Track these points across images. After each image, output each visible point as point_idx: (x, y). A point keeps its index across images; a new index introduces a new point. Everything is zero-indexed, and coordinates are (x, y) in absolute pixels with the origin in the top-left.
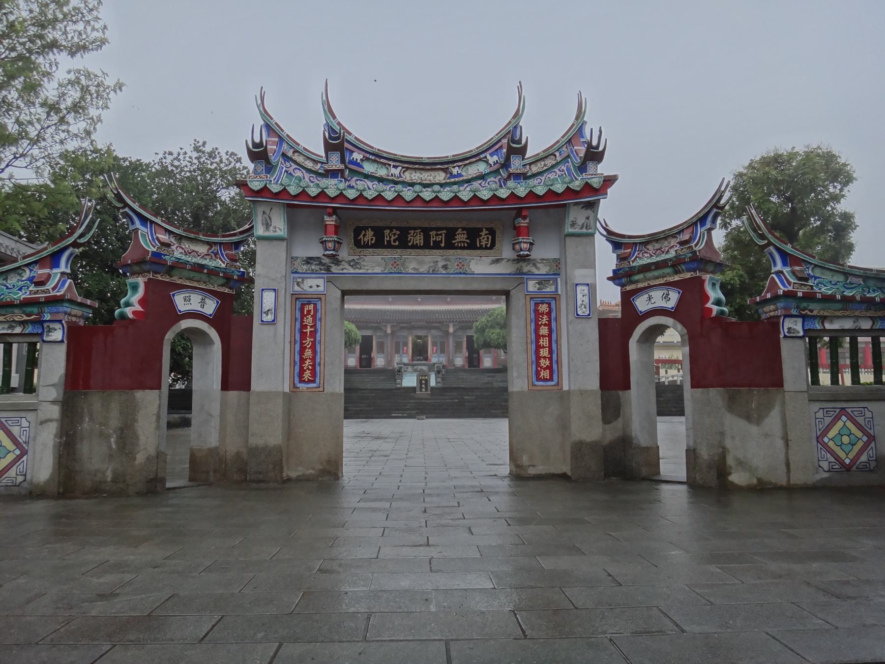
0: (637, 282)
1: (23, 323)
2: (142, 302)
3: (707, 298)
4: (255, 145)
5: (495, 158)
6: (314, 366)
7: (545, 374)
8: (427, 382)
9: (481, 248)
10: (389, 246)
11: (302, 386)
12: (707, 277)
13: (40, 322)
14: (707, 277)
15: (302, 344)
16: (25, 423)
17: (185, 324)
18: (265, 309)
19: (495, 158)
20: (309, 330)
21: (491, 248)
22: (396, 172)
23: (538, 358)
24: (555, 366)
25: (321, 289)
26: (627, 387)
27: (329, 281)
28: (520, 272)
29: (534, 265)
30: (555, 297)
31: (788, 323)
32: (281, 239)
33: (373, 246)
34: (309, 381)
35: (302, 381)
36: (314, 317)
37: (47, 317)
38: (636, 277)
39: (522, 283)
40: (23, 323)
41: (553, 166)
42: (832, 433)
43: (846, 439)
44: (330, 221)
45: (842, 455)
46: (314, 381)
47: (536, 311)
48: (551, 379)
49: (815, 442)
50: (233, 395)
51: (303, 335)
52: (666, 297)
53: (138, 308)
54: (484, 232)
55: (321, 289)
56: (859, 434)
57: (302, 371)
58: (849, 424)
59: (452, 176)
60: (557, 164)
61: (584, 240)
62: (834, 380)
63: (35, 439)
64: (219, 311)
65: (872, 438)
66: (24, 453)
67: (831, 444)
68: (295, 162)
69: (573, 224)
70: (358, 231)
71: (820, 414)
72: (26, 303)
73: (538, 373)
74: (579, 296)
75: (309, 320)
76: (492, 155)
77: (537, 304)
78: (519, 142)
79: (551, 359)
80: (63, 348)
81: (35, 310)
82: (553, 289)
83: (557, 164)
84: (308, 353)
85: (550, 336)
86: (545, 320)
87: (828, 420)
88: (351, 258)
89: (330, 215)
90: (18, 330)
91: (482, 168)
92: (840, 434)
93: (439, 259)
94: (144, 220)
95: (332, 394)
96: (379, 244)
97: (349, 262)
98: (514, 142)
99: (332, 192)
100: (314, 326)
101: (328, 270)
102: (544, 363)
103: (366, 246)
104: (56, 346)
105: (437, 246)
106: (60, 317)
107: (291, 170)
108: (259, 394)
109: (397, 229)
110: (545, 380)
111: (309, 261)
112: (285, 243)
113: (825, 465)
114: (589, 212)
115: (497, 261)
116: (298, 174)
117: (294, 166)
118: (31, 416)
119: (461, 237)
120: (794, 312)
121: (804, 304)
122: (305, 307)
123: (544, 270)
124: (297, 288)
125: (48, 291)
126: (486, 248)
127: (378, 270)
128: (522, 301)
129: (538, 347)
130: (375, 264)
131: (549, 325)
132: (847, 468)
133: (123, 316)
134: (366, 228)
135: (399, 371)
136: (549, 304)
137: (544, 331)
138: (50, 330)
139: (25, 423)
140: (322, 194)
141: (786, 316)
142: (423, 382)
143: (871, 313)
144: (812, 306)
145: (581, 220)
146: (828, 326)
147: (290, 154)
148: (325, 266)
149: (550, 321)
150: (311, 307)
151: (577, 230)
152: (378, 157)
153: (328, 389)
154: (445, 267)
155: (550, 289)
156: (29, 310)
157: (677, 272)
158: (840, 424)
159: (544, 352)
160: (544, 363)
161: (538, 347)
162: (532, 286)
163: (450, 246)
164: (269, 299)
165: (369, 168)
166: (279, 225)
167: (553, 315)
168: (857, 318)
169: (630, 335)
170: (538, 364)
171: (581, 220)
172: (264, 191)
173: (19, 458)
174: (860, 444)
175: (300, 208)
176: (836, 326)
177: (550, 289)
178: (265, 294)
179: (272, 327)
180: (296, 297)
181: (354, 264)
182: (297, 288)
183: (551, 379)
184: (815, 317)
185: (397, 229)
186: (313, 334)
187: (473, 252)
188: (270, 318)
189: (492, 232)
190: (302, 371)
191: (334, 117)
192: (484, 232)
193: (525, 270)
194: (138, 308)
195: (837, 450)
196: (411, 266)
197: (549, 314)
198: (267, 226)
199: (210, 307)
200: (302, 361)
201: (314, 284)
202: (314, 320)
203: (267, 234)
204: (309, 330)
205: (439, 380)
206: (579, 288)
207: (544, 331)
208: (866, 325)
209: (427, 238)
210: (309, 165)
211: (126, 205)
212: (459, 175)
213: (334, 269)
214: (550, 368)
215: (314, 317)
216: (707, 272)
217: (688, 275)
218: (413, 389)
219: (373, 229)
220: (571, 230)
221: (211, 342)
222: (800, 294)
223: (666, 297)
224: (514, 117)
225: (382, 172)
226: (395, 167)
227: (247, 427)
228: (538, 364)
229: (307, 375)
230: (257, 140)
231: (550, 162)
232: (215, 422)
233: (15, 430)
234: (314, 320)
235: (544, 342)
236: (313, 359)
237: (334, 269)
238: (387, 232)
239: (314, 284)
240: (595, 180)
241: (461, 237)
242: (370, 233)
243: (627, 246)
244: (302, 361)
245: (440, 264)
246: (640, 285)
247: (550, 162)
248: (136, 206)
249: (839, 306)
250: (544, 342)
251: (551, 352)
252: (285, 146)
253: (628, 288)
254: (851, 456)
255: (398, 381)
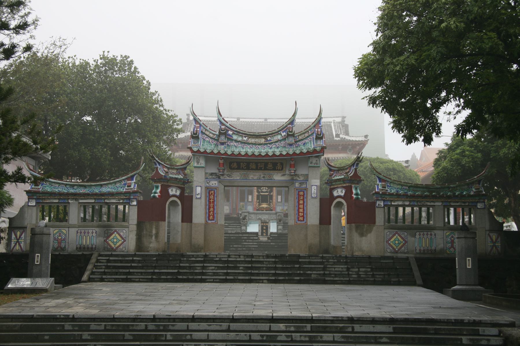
0: (334, 185)
1: (123, 199)
2: (160, 192)
3: (353, 193)
4: (194, 134)
5: (285, 133)
6: (214, 214)
7: (301, 219)
8: (267, 228)
9: (278, 170)
10: (243, 169)
11: (209, 222)
12: (353, 186)
13: (129, 199)
14: (353, 186)
15: (209, 206)
16: (125, 232)
17: (171, 199)
18: (197, 193)
19: (285, 133)
20: (212, 200)
21: (282, 169)
22: (245, 139)
23: (299, 212)
24: (305, 216)
25: (217, 185)
26: (330, 224)
27: (219, 182)
28: (292, 179)
29: (298, 177)
30: (306, 189)
31: (378, 203)
32: (203, 167)
33: (237, 169)
34: (212, 220)
35: (209, 220)
36: (214, 196)
37: (132, 197)
38: (334, 183)
39: (293, 184)
40: (123, 199)
41: (308, 137)
42: (392, 240)
43: (397, 242)
44: (221, 162)
45: (395, 247)
46: (214, 220)
47: (299, 194)
48: (303, 220)
49: (385, 243)
50: (185, 224)
51: (210, 203)
52: (176, 191)
53: (159, 194)
54: (279, 164)
55: (217, 185)
56: (402, 240)
57: (209, 216)
58: (399, 237)
59: (267, 140)
60: (309, 136)
61: (316, 169)
62: (428, 222)
63: (128, 237)
64: (181, 194)
65: (406, 242)
66: (125, 241)
67: (391, 243)
68: (206, 135)
69: (311, 163)
70: (231, 163)
71: (388, 233)
72: (126, 193)
73: (298, 218)
74: (313, 190)
75: (212, 197)
76: (283, 132)
77: (299, 192)
78: (292, 132)
79: (303, 213)
80: (136, 207)
81: (128, 195)
82: (305, 186)
83: (309, 136)
84: (212, 209)
85: (303, 204)
86: (302, 198)
87: (391, 236)
88: (228, 173)
89: (221, 160)
90: (121, 201)
91: (279, 137)
92: (395, 240)
93: (261, 174)
94: (159, 164)
95: (221, 225)
96: (239, 168)
97: (227, 175)
98: (290, 132)
99: (222, 152)
100: (214, 199)
101: (219, 178)
102: (301, 214)
103: (234, 169)
104: (134, 207)
105: (261, 169)
106: (136, 197)
107: (204, 138)
108: (195, 224)
109: (246, 162)
110: (301, 221)
111: (212, 174)
112: (204, 169)
113: (389, 250)
114: (317, 159)
115: (284, 175)
116: (207, 139)
117: (206, 136)
118: (127, 229)
119: (270, 166)
120: (380, 199)
121: (383, 196)
122: (210, 192)
123: (302, 178)
124: (207, 185)
125: (132, 189)
126: (280, 170)
127: (238, 178)
128: (293, 191)
129: (299, 208)
130: (237, 176)
131: (303, 200)
132: (397, 252)
133: (154, 197)
134: (234, 162)
135: (244, 219)
136: (304, 192)
137: (301, 202)
138: (132, 201)
139: (125, 232)
140: (219, 153)
141: (377, 200)
142: (264, 228)
143: (408, 199)
144: (386, 197)
145: (314, 162)
146: (393, 203)
147: (204, 131)
148: (217, 176)
149: (304, 198)
150: (213, 192)
151: (313, 165)
152: (238, 133)
153: (219, 223)
154: (264, 177)
155: (304, 186)
156: (126, 195)
157: (345, 183)
158: (395, 237)
159: (301, 210)
160: (301, 214)
161: (299, 208)
162: (297, 185)
163: (266, 169)
164: (199, 190)
165: (235, 137)
166: (202, 163)
167: (305, 196)
168: (404, 201)
169: (331, 205)
170: (299, 215)
171: (314, 162)
172: (198, 151)
173: (404, 244)
174: (402, 244)
175: (210, 157)
176: (396, 203)
177: (304, 186)
178: (197, 188)
179: (199, 200)
180: (207, 188)
181: (229, 176)
182: (207, 185)
183: (303, 220)
184: (388, 200)
185: (246, 162)
186: (213, 202)
187: (275, 171)
188: (199, 196)
189: (282, 164)
190: (209, 216)
191: (221, 116)
192: (279, 164)
193: (295, 178)
194: (159, 194)
195: (394, 246)
196: (251, 177)
197: (303, 196)
198: (198, 163)
199: (178, 193)
200: (209, 212)
201: (214, 183)
202: (214, 197)
203: (198, 166)
204: (212, 200)
205: (280, 227)
206: (313, 187)
207: (301, 202)
208: (407, 203)
209: (257, 166)
210: (211, 135)
211: (155, 159)
212: (270, 140)
213: (222, 178)
214: (303, 216)
215: (214, 196)
216: (354, 183)
217: (347, 185)
218: (256, 234)
219: (237, 162)
220: (311, 165)
221: (178, 205)
222: (381, 193)
223: (176, 191)
224: (293, 116)
225: (240, 139)
226: (245, 137)
227: (191, 236)
228: (299, 215)
229: (211, 218)
230: (195, 132)
231: (306, 135)
232: (180, 233)
233: (122, 234)
234: (214, 197)
235: (301, 206)
236: (214, 212)
237: (222, 178)
238: (242, 164)
239: (214, 183)
240: (318, 148)
241: (270, 166)
242: (235, 164)
243: (334, 171)
244: (209, 212)
245: (262, 176)
246: (335, 186)
247: (306, 135)
248: (157, 159)
249: (396, 197)
250: (301, 206)
251: (304, 210)
252: (202, 128)
253: (332, 187)
254: (398, 248)
255: (243, 228)
